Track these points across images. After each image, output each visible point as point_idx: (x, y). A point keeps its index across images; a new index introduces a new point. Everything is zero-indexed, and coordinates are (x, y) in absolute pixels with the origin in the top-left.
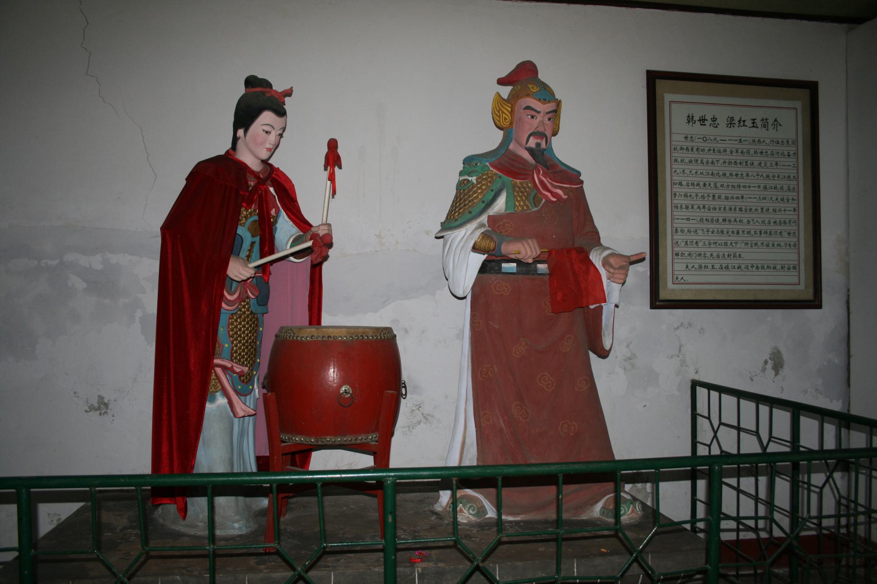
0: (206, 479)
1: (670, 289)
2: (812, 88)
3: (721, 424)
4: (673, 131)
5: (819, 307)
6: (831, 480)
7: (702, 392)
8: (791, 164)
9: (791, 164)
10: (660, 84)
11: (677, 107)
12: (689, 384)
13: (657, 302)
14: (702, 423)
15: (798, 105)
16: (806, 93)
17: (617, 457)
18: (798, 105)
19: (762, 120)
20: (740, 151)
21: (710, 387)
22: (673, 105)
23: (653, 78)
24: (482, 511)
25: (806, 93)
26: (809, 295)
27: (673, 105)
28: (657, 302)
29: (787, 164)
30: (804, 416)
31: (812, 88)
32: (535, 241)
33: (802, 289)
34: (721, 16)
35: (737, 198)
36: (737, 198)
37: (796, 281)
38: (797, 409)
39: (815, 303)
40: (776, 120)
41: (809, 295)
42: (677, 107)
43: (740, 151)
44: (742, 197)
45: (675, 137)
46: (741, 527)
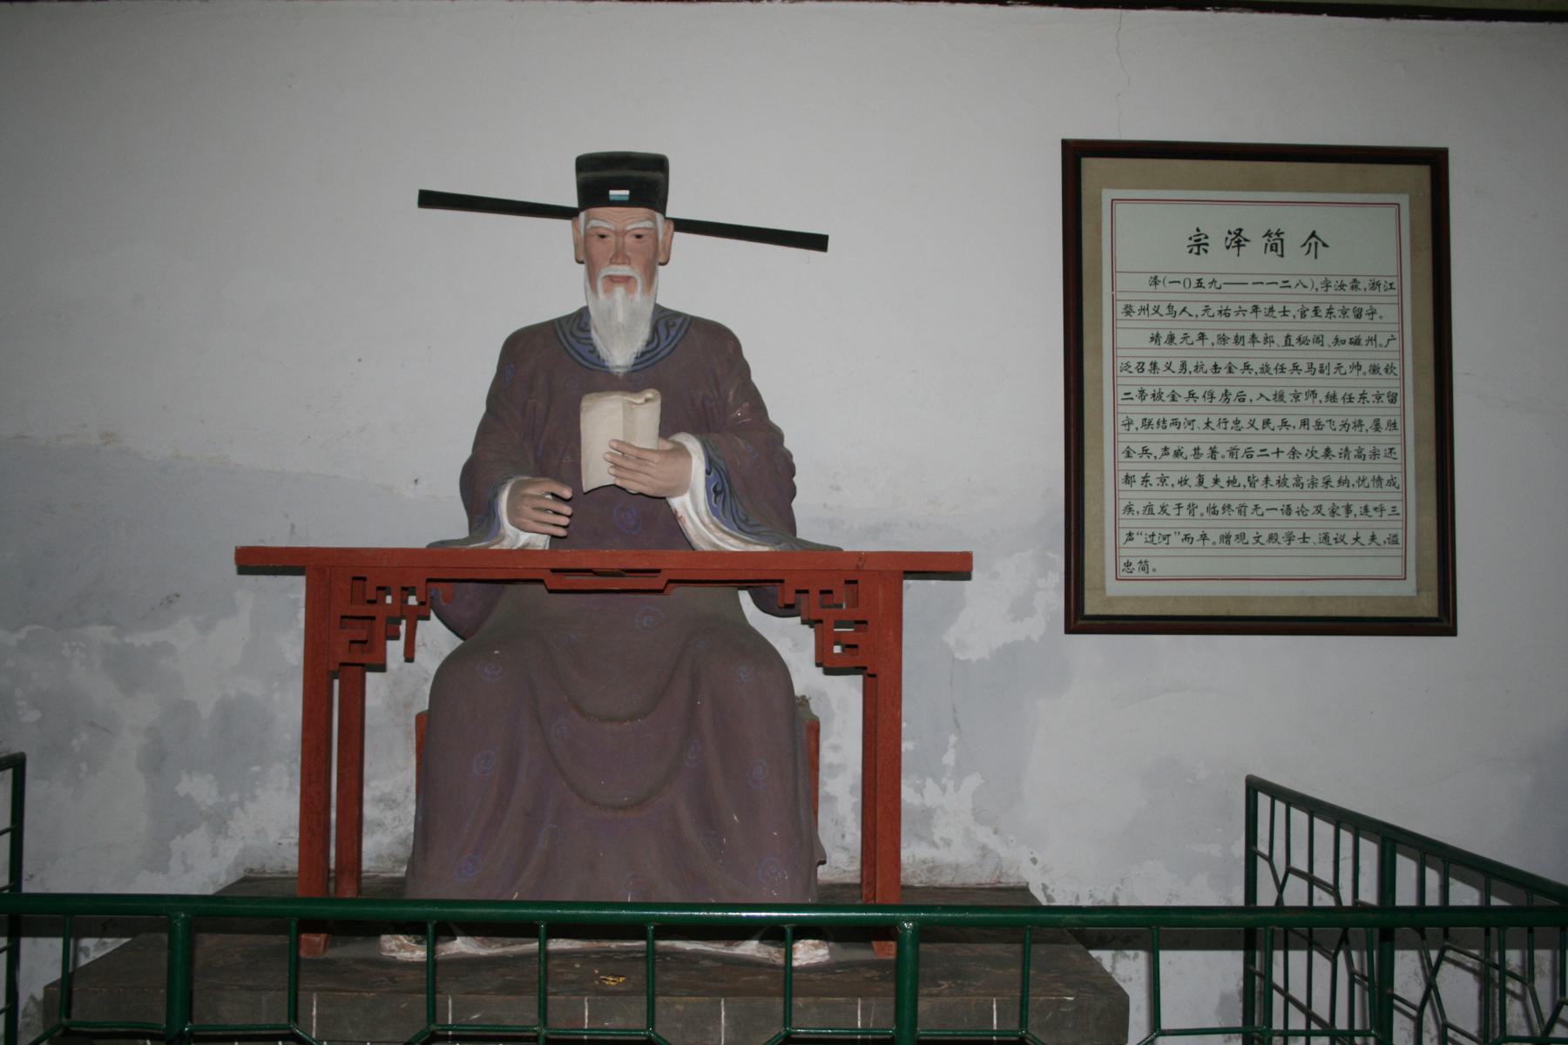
0: (428, 909)
1: (1111, 590)
2: (1435, 161)
3: (1290, 870)
5: (1451, 631)
6: (1450, 1033)
7: (1263, 800)
10: (1091, 167)
11: (1144, 230)
12: (15, 749)
14: (1262, 865)
15: (1404, 200)
16: (1423, 173)
19: (1268, 234)
21: (1276, 792)
22: (1119, 207)
23: (1075, 154)
25: (1423, 173)
26: (1428, 606)
30: (1403, 854)
32: (588, 396)
33: (1398, 582)
37: (1398, 572)
38: (1392, 840)
40: (1313, 235)
41: (1428, 606)
42: (1144, 230)
46: (1314, 1027)
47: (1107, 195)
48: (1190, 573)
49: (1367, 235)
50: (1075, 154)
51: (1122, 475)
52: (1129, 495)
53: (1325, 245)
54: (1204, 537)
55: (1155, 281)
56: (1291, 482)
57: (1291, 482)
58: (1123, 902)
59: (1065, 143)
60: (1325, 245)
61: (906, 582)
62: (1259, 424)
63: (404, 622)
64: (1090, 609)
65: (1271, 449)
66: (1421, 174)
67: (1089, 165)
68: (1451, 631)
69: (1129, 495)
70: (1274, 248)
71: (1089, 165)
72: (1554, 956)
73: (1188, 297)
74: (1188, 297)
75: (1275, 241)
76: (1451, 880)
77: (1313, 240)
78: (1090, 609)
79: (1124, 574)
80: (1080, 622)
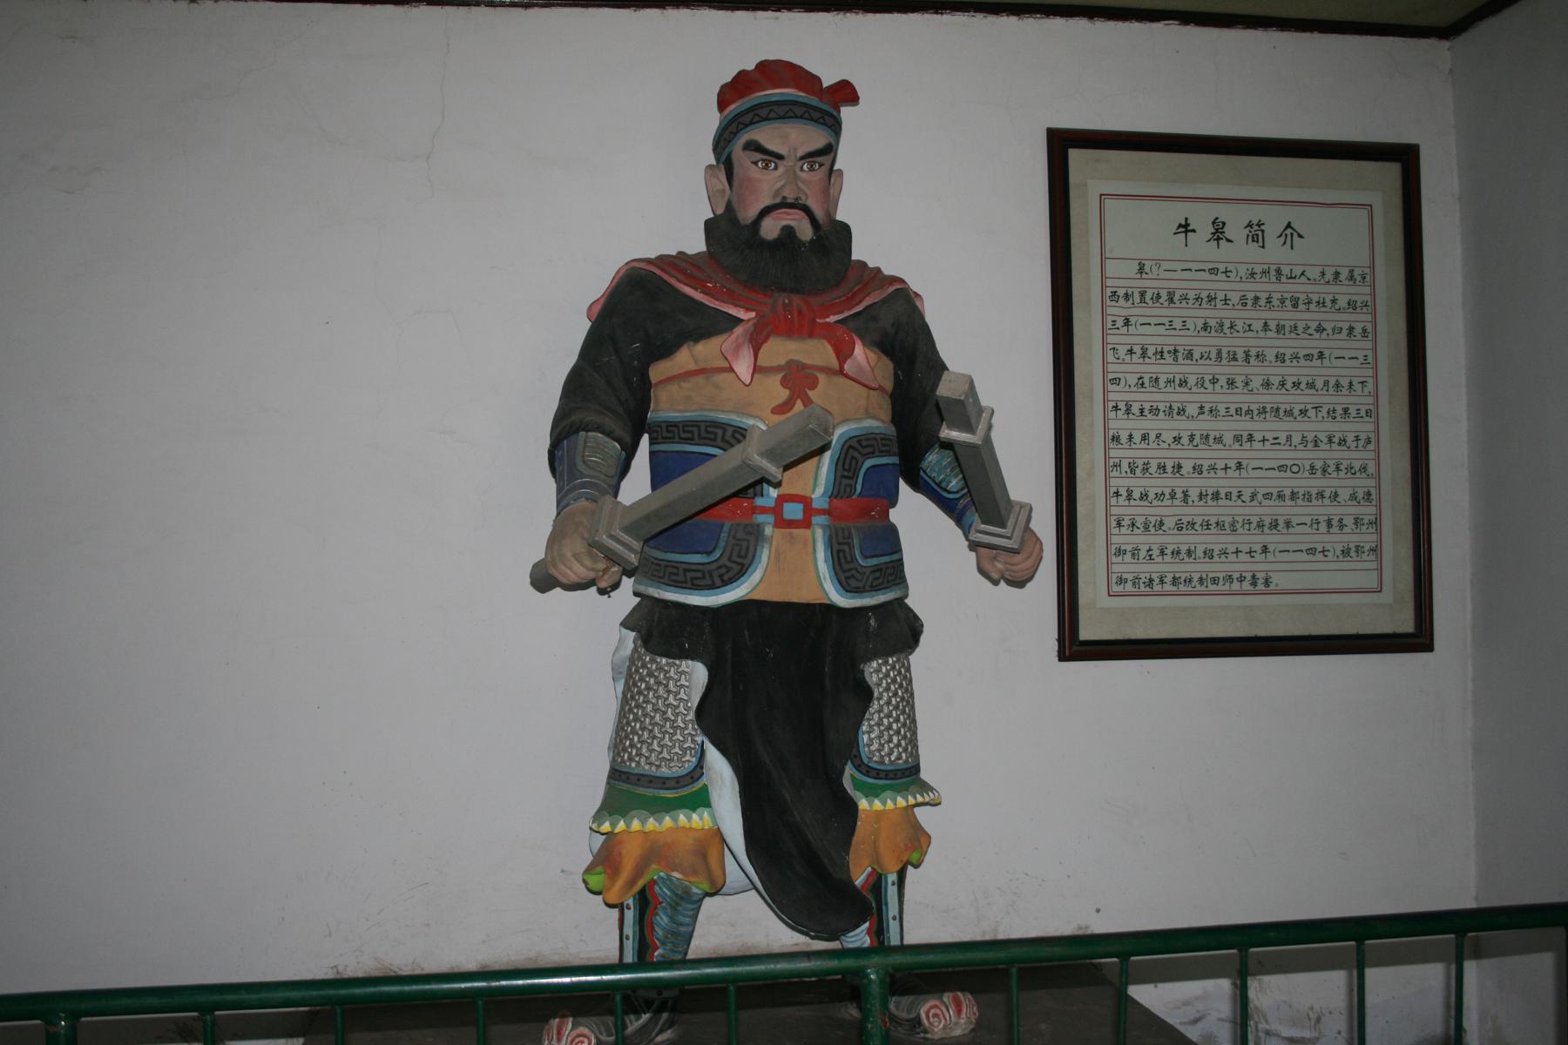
2: (1405, 157)
5: (1428, 647)
8: (1360, 354)
9: (1360, 354)
11: (1131, 223)
13: (1073, 647)
15: (1376, 199)
16: (1393, 170)
17: (704, 248)
19: (1250, 225)
20: (1126, 522)
23: (1061, 143)
24: (897, 1005)
25: (1393, 170)
26: (1404, 623)
27: (1108, 203)
28: (1073, 647)
29: (1347, 354)
31: (1405, 157)
34: (1158, 27)
35: (1308, 357)
36: (1308, 357)
39: (1419, 640)
40: (1289, 226)
43: (1126, 522)
44: (1321, 356)
45: (1112, 268)
49: (1340, 227)
50: (1061, 143)
58: (1001, 936)
63: (1142, 993)
64: (1085, 634)
66: (1391, 172)
67: (1077, 158)
68: (1428, 647)
70: (1255, 239)
71: (1077, 158)
72: (1350, 977)
75: (1256, 233)
76: (690, 956)
77: (1289, 231)
78: (1085, 634)
79: (1116, 588)
80: (1075, 648)
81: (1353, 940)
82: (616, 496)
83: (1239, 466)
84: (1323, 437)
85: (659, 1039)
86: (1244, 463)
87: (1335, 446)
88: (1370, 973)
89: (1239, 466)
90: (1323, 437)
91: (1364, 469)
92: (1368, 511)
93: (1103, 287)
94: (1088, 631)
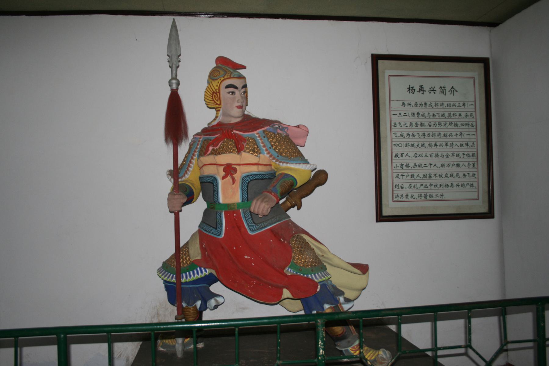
4: (392, 98)
5: (492, 217)
13: (381, 218)
15: (475, 74)
18: (475, 74)
19: (441, 88)
22: (391, 78)
23: (376, 59)
27: (391, 78)
37: (476, 197)
40: (452, 88)
47: (388, 73)
48: (473, 96)
50: (376, 59)
51: (394, 154)
52: (396, 150)
53: (456, 91)
54: (460, 115)
55: (403, 104)
56: (444, 176)
57: (444, 176)
59: (377, 221)
60: (456, 91)
61: (288, 212)
62: (461, 104)
65: (454, 134)
69: (396, 150)
70: (443, 92)
73: (408, 150)
74: (408, 150)
77: (452, 89)
79: (395, 200)
81: (466, 310)
82: (184, 204)
83: (461, 134)
84: (450, 154)
85: (318, 290)
86: (463, 133)
87: (455, 157)
88: (473, 321)
89: (461, 134)
90: (450, 154)
91: (471, 115)
92: (472, 160)
93: (476, 129)
94: (386, 212)
